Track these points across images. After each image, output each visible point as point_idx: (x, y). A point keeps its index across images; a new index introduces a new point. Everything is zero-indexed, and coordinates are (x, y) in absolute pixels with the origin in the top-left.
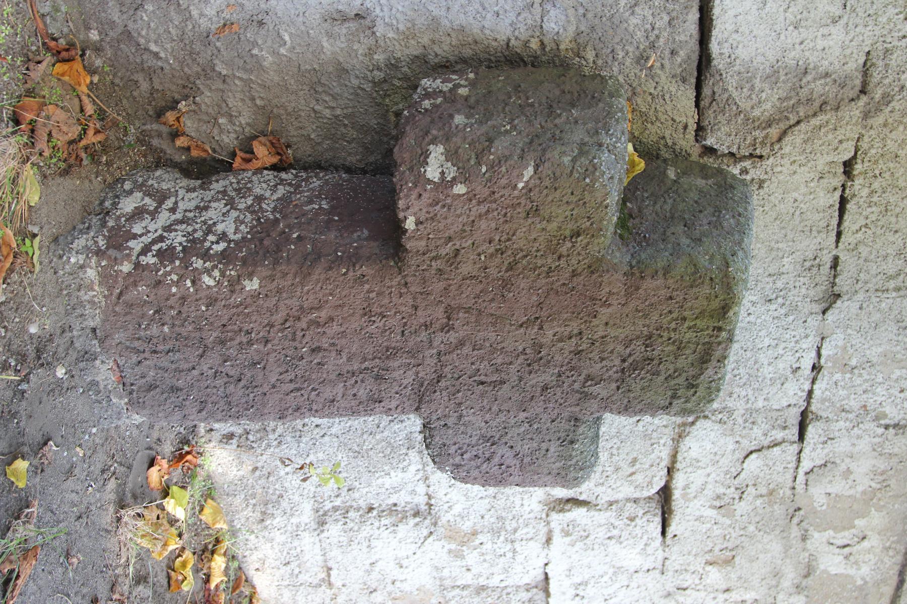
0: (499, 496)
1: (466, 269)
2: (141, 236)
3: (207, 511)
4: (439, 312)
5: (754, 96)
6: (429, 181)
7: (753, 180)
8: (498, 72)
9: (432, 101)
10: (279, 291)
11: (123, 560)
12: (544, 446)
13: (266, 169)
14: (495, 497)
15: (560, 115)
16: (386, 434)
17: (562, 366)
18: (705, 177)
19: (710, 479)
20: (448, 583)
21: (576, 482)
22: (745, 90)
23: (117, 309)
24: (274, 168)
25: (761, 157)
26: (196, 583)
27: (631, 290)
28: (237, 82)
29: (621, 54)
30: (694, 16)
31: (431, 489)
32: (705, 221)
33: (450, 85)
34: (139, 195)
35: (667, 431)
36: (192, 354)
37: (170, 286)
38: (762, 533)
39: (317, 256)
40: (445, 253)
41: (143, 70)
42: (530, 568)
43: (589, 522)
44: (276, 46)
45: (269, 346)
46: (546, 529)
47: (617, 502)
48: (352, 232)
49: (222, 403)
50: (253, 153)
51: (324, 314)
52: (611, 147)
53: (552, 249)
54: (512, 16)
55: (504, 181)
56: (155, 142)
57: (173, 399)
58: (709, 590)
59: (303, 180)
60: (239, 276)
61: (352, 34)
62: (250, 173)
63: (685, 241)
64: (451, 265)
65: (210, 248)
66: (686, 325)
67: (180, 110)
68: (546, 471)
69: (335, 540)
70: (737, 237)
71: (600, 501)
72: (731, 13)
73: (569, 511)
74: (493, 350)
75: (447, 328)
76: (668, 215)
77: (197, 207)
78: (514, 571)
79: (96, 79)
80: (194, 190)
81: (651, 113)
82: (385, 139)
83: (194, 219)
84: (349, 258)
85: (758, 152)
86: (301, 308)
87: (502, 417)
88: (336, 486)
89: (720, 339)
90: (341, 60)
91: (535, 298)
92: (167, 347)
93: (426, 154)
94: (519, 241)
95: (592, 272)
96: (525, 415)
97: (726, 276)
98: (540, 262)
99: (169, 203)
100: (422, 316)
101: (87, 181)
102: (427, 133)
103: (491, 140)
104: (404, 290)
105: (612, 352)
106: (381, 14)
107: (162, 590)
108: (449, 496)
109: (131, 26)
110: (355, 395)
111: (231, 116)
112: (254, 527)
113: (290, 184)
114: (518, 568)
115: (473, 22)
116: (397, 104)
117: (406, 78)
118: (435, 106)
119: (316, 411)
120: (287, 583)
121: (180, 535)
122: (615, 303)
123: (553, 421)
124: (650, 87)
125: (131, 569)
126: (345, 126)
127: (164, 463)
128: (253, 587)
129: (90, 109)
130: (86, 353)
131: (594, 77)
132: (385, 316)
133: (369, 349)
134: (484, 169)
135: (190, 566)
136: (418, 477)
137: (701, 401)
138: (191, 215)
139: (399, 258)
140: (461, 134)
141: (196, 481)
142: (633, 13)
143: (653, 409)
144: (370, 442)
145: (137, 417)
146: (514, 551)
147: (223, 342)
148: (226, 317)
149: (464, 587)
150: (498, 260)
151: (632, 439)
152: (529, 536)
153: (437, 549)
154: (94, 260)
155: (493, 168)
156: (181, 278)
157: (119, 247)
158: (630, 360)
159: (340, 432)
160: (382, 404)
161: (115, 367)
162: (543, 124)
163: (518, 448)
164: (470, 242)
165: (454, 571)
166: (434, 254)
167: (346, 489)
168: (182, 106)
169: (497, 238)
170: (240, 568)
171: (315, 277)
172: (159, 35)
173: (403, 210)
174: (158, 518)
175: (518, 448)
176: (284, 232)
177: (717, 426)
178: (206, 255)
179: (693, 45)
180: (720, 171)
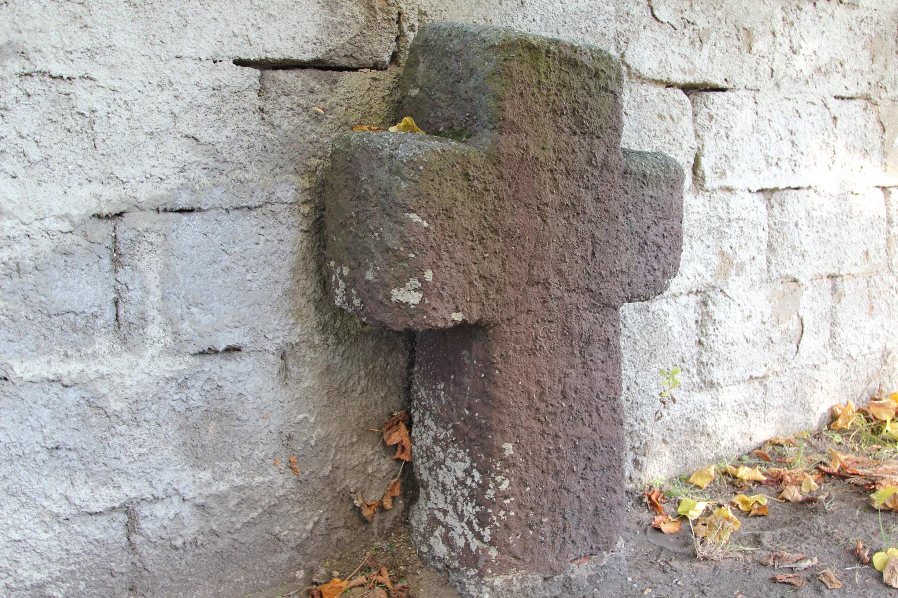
0: (690, 233)
1: (496, 269)
2: (467, 540)
3: (699, 482)
4: (533, 291)
5: (348, 22)
6: (422, 301)
7: (419, 20)
8: (329, 241)
9: (354, 297)
10: (514, 426)
11: (741, 556)
12: (648, 200)
13: (410, 434)
14: (691, 237)
15: (366, 190)
16: (635, 330)
17: (579, 186)
18: (417, 63)
19: (677, 51)
20: (765, 276)
21: (679, 172)
22: (343, 30)
23: (528, 560)
24: (409, 426)
25: (399, 14)
26: (761, 493)
27: (515, 128)
28: (338, 458)
29: (313, 136)
30: (281, 74)
31: (683, 291)
32: (455, 65)
33: (341, 282)
34: (432, 540)
35: (635, 89)
36: (566, 498)
37: (509, 517)
38: (724, 5)
39: (485, 395)
40: (483, 288)
41: (328, 535)
42: (753, 205)
43: (713, 155)
44: (308, 426)
45: (560, 434)
46: (719, 192)
47: (696, 131)
48: (465, 364)
49: (608, 473)
50: (397, 444)
51: (534, 389)
52: (393, 147)
53: (479, 196)
54: (282, 228)
55: (422, 239)
56: (388, 525)
57: (604, 514)
58: (773, 50)
59: (420, 403)
60: (501, 460)
61: (298, 362)
62: (414, 447)
63: (472, 83)
64: (493, 282)
65: (478, 483)
66: (544, 81)
67: (362, 505)
68: (669, 198)
69: (727, 373)
70: (469, 38)
71: (695, 146)
72: (278, 43)
73: (703, 172)
74: (565, 245)
75: (546, 285)
76: (450, 96)
77: (443, 492)
78: (755, 219)
79: (336, 573)
80: (428, 494)
81: (362, 109)
82: (385, 333)
83: (454, 496)
84: (486, 367)
85: (395, 17)
86: (528, 407)
87: (623, 236)
88: (680, 373)
89: (556, 51)
90: (319, 371)
91: (521, 210)
92: (561, 519)
93: (399, 304)
94: (473, 224)
95: (499, 162)
96: (621, 217)
97: (502, 47)
98: (491, 207)
99: (439, 515)
100: (536, 306)
101: (421, 582)
102: (381, 303)
103: (388, 250)
104: (514, 321)
105: (567, 144)
106: (281, 338)
107: (767, 522)
108: (690, 276)
109: (292, 544)
110: (603, 362)
111: (366, 462)
112: (714, 442)
113: (424, 414)
114: (753, 215)
115: (287, 262)
116: (356, 324)
117: (334, 317)
118: (358, 295)
119: (616, 394)
120: (762, 414)
121: (720, 506)
122: (525, 142)
123: (626, 192)
124: (340, 110)
125: (748, 549)
126: (374, 367)
127: (658, 519)
128: (765, 442)
129: (361, 579)
130: (564, 585)
131: (333, 160)
132: (536, 338)
133: (564, 350)
134: (412, 255)
135: (746, 498)
136: (673, 302)
137: (610, 66)
138: (449, 498)
139: (487, 325)
140: (382, 275)
141: (673, 491)
142: (279, 127)
143: (616, 107)
144: (642, 344)
145: (619, 544)
146: (738, 219)
147: (557, 473)
148: (535, 470)
149: (769, 262)
150: (489, 243)
151: (642, 119)
152: (725, 206)
153: (736, 286)
154: (486, 579)
155: (410, 248)
156: (502, 507)
157: (476, 558)
158: (574, 127)
159: (634, 370)
160: (611, 338)
161: (577, 562)
162: (373, 205)
163: (650, 222)
164: (473, 266)
165: (754, 271)
166: (483, 297)
167: (682, 364)
168: (358, 503)
169: (470, 243)
170: (749, 454)
171: (502, 396)
172: (300, 521)
173: (446, 323)
174: (705, 525)
175: (650, 222)
176: (464, 421)
177: (631, 46)
178: (484, 487)
179: (305, 74)
180: (412, 50)
